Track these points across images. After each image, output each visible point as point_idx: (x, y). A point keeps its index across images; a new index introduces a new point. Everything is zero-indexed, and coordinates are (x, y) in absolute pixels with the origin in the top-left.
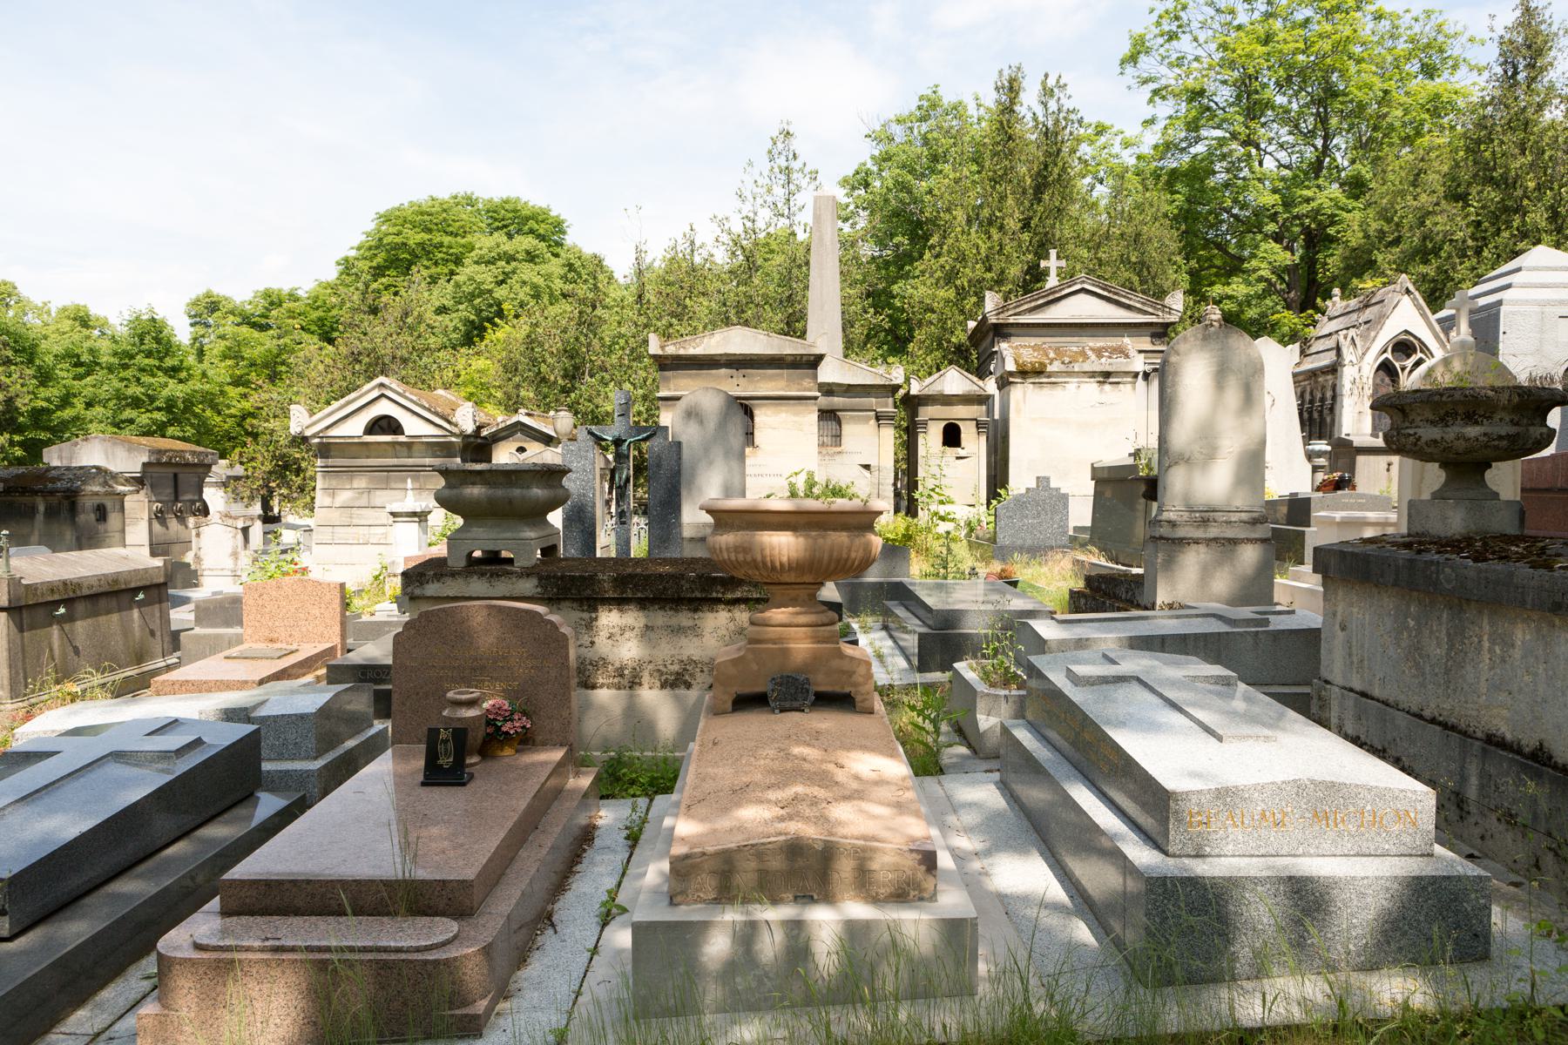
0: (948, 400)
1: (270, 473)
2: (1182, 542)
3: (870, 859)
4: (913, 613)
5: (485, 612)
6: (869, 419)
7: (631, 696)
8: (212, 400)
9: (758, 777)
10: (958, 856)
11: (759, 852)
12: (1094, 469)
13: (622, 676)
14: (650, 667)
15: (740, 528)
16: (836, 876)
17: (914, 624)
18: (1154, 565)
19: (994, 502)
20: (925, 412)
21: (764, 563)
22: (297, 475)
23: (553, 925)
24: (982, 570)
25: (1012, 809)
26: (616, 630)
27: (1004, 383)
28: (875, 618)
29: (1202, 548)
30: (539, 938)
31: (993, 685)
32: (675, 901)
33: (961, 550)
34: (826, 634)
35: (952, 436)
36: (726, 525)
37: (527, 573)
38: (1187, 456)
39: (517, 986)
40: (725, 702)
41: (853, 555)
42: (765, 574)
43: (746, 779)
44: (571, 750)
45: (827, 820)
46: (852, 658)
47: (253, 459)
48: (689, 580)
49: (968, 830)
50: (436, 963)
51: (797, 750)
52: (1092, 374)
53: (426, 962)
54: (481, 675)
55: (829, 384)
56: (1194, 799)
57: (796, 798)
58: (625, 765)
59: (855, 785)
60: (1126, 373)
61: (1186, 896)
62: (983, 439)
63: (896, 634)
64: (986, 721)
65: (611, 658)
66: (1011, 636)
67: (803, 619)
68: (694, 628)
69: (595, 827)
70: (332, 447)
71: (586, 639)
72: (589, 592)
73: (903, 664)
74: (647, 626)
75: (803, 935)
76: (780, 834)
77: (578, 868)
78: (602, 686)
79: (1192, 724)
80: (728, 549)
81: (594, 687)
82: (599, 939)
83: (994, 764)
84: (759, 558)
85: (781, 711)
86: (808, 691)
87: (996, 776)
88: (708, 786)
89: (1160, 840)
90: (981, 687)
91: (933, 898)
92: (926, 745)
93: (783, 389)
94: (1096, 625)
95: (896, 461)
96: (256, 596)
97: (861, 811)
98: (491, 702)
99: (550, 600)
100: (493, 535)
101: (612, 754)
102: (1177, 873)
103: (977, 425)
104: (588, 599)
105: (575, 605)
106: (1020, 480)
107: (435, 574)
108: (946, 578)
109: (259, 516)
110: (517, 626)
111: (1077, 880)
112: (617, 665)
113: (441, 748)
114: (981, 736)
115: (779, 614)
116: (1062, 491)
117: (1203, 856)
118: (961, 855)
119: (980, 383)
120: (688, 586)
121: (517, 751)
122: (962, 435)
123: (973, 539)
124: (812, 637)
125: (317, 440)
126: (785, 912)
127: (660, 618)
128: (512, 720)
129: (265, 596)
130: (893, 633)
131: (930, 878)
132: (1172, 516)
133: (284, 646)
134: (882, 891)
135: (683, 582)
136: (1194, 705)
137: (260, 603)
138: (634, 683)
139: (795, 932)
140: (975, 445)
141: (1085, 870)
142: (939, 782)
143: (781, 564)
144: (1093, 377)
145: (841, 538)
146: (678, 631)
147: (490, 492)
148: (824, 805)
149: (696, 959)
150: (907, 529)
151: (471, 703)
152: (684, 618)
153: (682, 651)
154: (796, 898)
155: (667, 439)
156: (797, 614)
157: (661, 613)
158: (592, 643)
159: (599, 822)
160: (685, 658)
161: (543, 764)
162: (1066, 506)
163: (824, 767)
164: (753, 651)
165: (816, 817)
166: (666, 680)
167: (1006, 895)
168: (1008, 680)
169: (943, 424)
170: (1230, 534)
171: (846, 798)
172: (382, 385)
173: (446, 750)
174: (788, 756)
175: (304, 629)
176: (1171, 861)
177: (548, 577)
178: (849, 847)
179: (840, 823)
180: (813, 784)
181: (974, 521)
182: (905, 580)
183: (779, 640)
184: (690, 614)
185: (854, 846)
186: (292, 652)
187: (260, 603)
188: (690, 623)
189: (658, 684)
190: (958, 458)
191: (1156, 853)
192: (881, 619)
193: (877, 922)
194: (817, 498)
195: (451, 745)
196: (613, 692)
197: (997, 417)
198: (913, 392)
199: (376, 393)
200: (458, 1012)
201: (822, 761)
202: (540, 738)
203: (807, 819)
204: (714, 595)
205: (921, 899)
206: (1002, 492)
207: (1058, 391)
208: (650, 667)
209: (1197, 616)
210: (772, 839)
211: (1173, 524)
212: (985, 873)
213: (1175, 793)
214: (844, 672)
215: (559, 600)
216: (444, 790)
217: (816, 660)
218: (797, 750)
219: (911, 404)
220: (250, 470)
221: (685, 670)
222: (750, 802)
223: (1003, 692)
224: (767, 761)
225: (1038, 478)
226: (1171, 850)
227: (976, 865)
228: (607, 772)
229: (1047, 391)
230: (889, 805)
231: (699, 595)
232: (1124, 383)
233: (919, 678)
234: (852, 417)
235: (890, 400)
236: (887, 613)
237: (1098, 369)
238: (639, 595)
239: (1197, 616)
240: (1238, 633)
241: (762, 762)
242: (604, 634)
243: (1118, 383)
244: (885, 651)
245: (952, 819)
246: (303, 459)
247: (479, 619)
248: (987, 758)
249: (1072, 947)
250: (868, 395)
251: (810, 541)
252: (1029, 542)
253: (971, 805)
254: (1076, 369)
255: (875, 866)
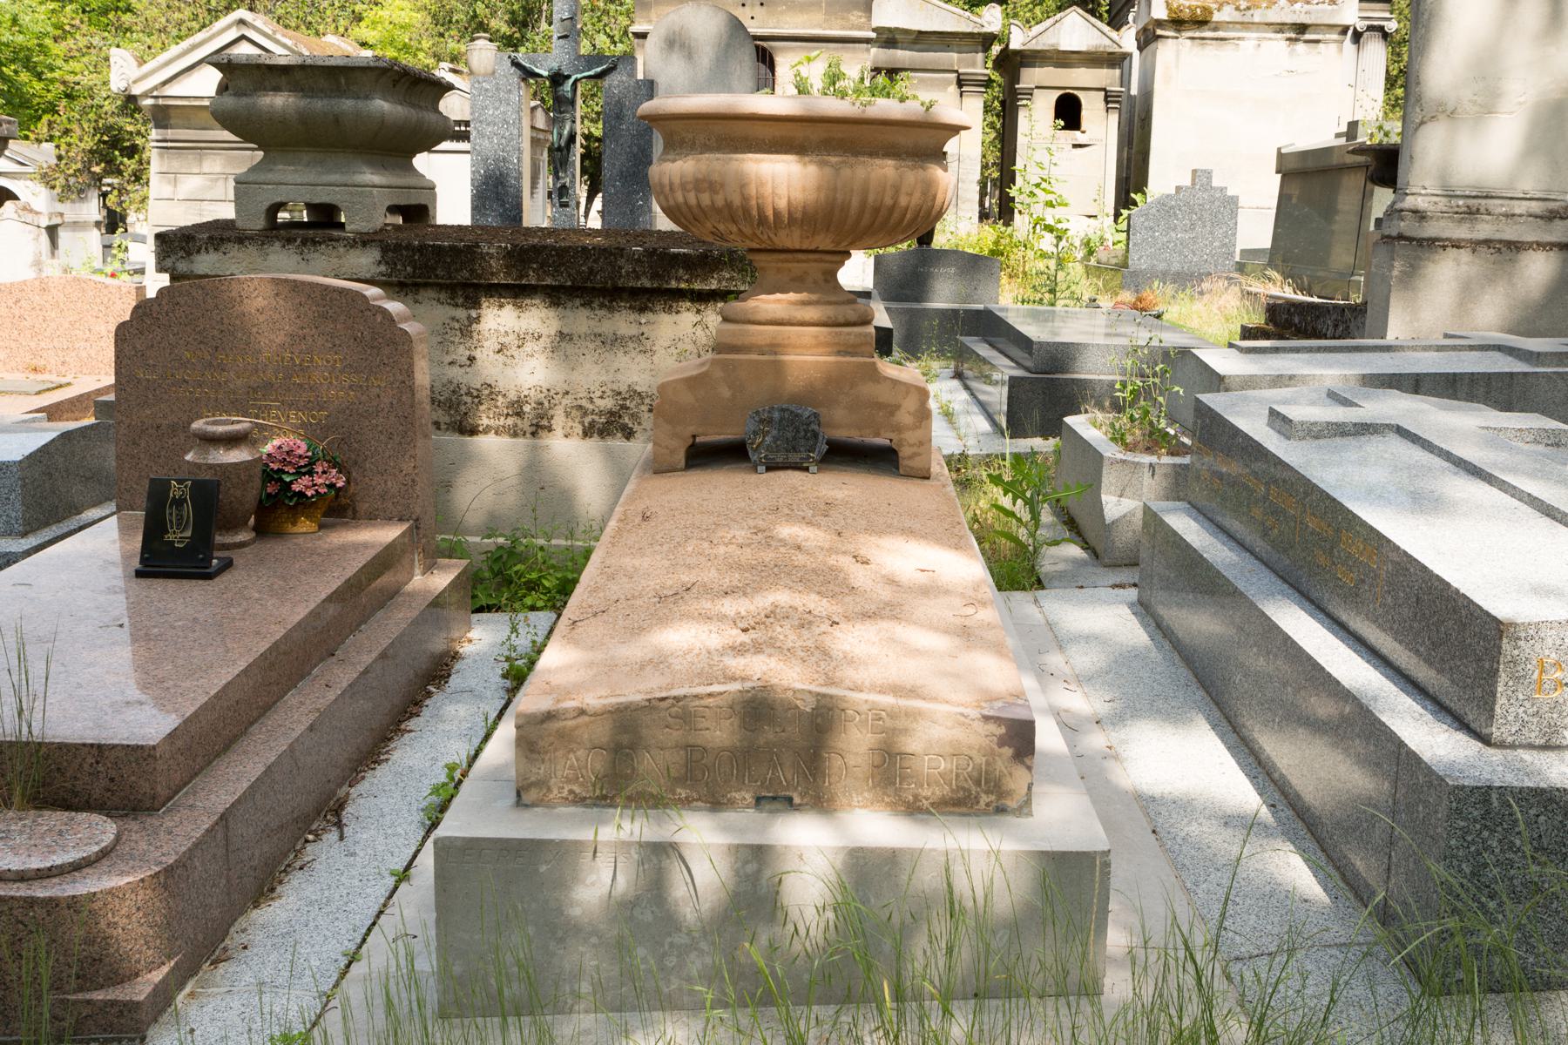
0: (1064, 59)
1: (91, 151)
2: (1432, 244)
3: (905, 731)
4: (1001, 352)
5: (270, 290)
6: (947, 83)
7: (535, 448)
8: (28, 59)
9: (710, 575)
10: (1070, 726)
11: (681, 711)
12: (1281, 156)
13: (519, 414)
14: (567, 401)
15: (706, 148)
16: (837, 762)
17: (1005, 369)
18: (1385, 280)
19: (1125, 212)
20: (1030, 77)
21: (746, 211)
22: (130, 157)
23: (340, 825)
24: (1105, 302)
25: (1160, 648)
26: (511, 340)
27: (1148, 38)
28: (943, 363)
29: (1465, 255)
30: (309, 847)
31: (1129, 448)
32: (526, 798)
33: (1076, 270)
34: (852, 339)
35: (1068, 112)
36: (682, 143)
37: (364, 241)
38: (1450, 108)
39: (244, 939)
40: (672, 452)
41: (903, 201)
42: (747, 231)
43: (687, 578)
44: (417, 526)
45: (826, 654)
46: (895, 382)
47: (67, 132)
48: (631, 258)
49: (1083, 680)
50: (52, 903)
51: (786, 531)
52: (1280, 27)
53: (31, 902)
54: (264, 397)
55: (889, 30)
56: (1551, 637)
57: (772, 614)
58: (522, 559)
59: (886, 594)
60: (1331, 27)
61: (1528, 824)
62: (1114, 118)
63: (974, 384)
64: (1117, 505)
65: (501, 386)
66: (1164, 372)
67: (812, 313)
68: (639, 338)
69: (456, 656)
70: (172, 113)
71: (462, 353)
72: (465, 273)
73: (984, 425)
74: (561, 335)
75: (767, 873)
76: (733, 679)
77: (412, 724)
78: (487, 430)
79: (1516, 503)
80: (683, 186)
81: (473, 432)
82: (415, 856)
83: (1125, 576)
84: (737, 201)
85: (769, 469)
86: (815, 435)
87: (1132, 594)
88: (615, 589)
89: (1471, 715)
90: (1111, 451)
91: (1025, 808)
92: (1015, 540)
93: (821, 27)
94: (1306, 356)
95: (985, 167)
96: (10, 303)
97: (892, 640)
98: (276, 442)
99: (398, 286)
100: (310, 176)
101: (501, 540)
102: (1511, 780)
103: (1106, 97)
104: (465, 286)
105: (443, 296)
106: (1163, 177)
107: (211, 238)
108: (1053, 305)
109: (98, 224)
110: (324, 316)
111: (1282, 776)
112: (512, 396)
113: (171, 514)
114: (1108, 528)
115: (771, 304)
116: (1230, 193)
117: (1559, 748)
118: (1071, 722)
119: (1114, 34)
120: (629, 267)
121: (321, 527)
122: (1083, 113)
123: (1093, 262)
124: (828, 344)
125: (149, 102)
126: (745, 824)
127: (582, 320)
128: (310, 473)
129: (23, 302)
130: (969, 383)
131: (1020, 773)
132: (1421, 203)
133: (46, 377)
134: (926, 792)
135: (621, 262)
136: (1514, 470)
137: (17, 313)
138: (540, 427)
139: (751, 868)
140: (1100, 125)
141: (1284, 751)
142: (1036, 601)
143: (776, 213)
144: (1281, 31)
145: (885, 169)
146: (614, 342)
147: (303, 103)
148: (825, 627)
149: (559, 911)
150: (997, 243)
151: (233, 440)
152: (623, 322)
153: (619, 376)
154: (759, 800)
155: (633, 73)
156: (804, 303)
157: (584, 313)
158: (472, 359)
159: (466, 649)
160: (624, 388)
161: (357, 547)
162: (1234, 214)
163: (832, 561)
164: (724, 365)
165: (806, 649)
166: (592, 424)
167: (1153, 799)
168: (1155, 441)
169: (1057, 94)
170: (1510, 233)
171: (867, 616)
172: (242, 22)
173: (180, 517)
174: (769, 541)
175: (84, 354)
176: (1495, 755)
177: (398, 248)
178: (865, 708)
179: (850, 661)
180: (809, 589)
181: (1095, 239)
182: (991, 306)
183: (774, 348)
184: (633, 316)
185: (874, 707)
186: (61, 386)
187: (17, 313)
188: (633, 330)
189: (579, 429)
190: (1075, 146)
191: (1461, 738)
192: (952, 364)
193: (916, 855)
194: (843, 95)
195: (188, 510)
196: (506, 440)
197: (1134, 91)
198: (1015, 45)
199: (233, 34)
200: (99, 996)
201: (831, 551)
202: (363, 507)
203: (787, 653)
204: (673, 284)
205: (1001, 810)
206: (1138, 197)
207: (1228, 48)
208: (567, 401)
209: (1472, 348)
210: (716, 688)
211: (1420, 215)
212: (1111, 754)
213: (1513, 624)
214: (880, 406)
215: (417, 287)
216: (171, 584)
217: (836, 382)
218: (786, 531)
219: (1011, 63)
220: (63, 147)
221: (624, 407)
222: (686, 616)
223: (1147, 459)
224: (732, 548)
225: (1194, 172)
226: (1496, 733)
227: (1096, 741)
228: (491, 569)
229: (1211, 50)
230: (946, 632)
231: (648, 284)
232: (1326, 42)
233: (1011, 446)
234: (921, 80)
235: (980, 56)
236: (963, 354)
237: (1290, 19)
238: (549, 281)
239: (1472, 348)
240: (1545, 375)
241: (722, 550)
242: (490, 345)
243: (1317, 41)
244: (956, 407)
245: (1055, 660)
246: (139, 133)
247: (260, 302)
248: (1115, 566)
249: (1279, 898)
250: (947, 48)
251: (828, 171)
252: (1176, 267)
253: (1088, 638)
254: (1257, 19)
255: (913, 744)
